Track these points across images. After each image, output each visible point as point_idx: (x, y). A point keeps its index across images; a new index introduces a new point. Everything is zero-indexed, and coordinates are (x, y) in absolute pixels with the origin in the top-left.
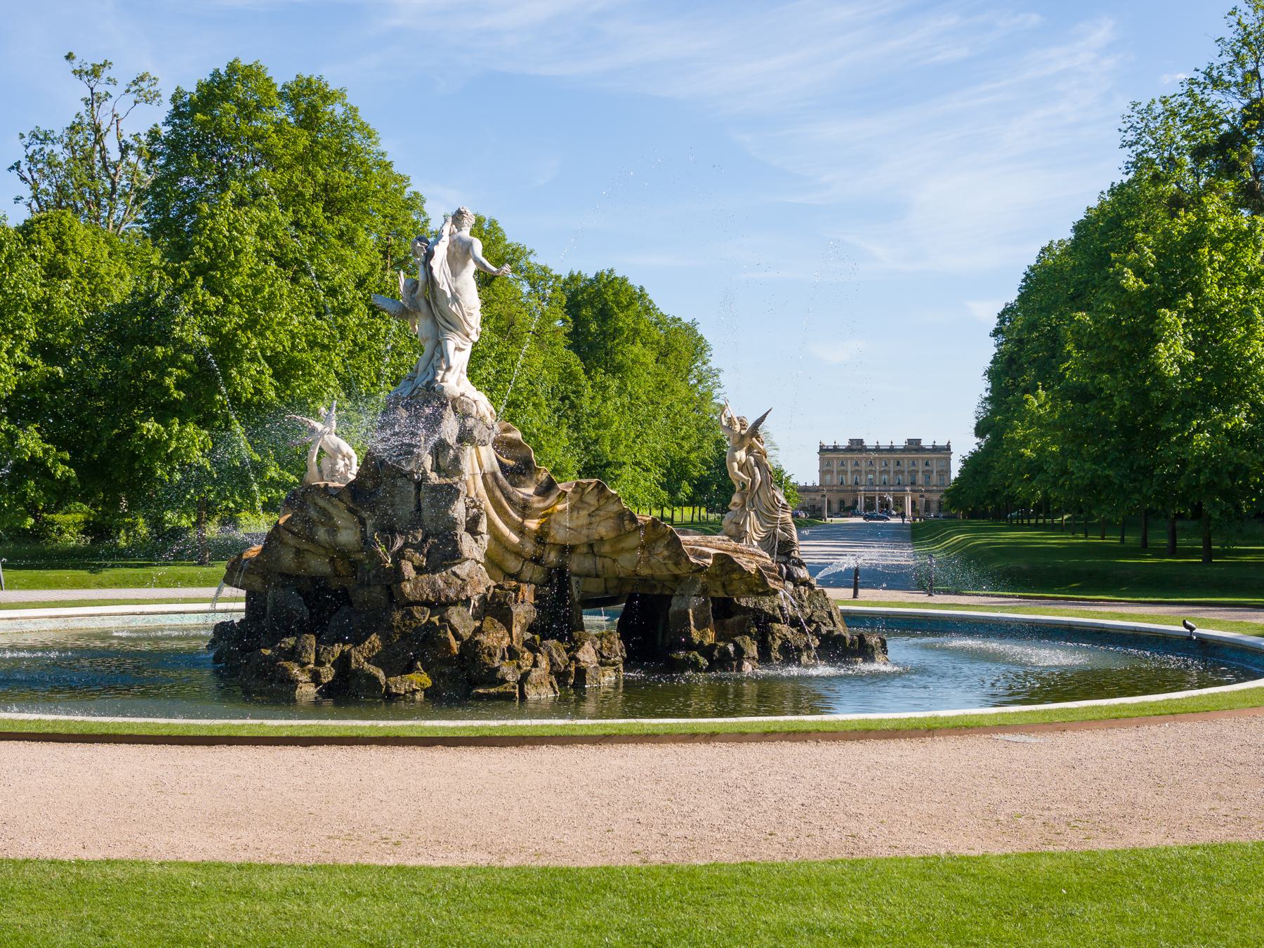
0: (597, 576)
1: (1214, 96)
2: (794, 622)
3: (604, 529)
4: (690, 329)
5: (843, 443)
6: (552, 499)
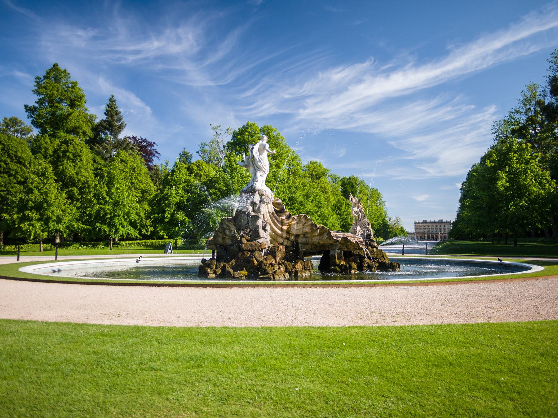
0: (307, 244)
1: (517, 116)
2: (369, 258)
3: (307, 229)
4: (376, 191)
5: (421, 221)
6: (290, 220)
